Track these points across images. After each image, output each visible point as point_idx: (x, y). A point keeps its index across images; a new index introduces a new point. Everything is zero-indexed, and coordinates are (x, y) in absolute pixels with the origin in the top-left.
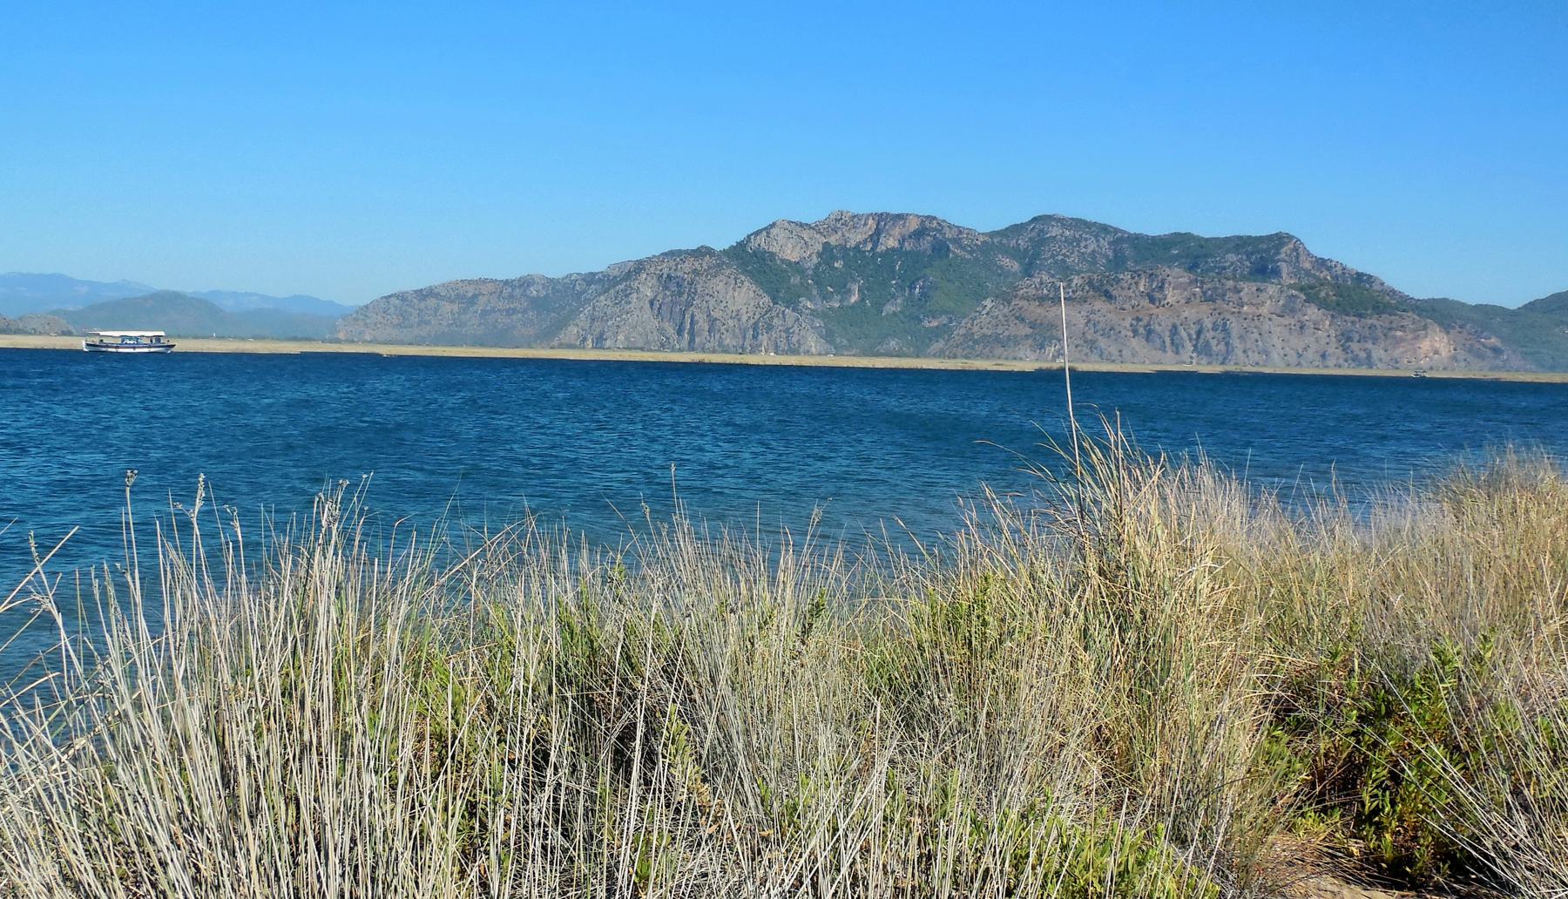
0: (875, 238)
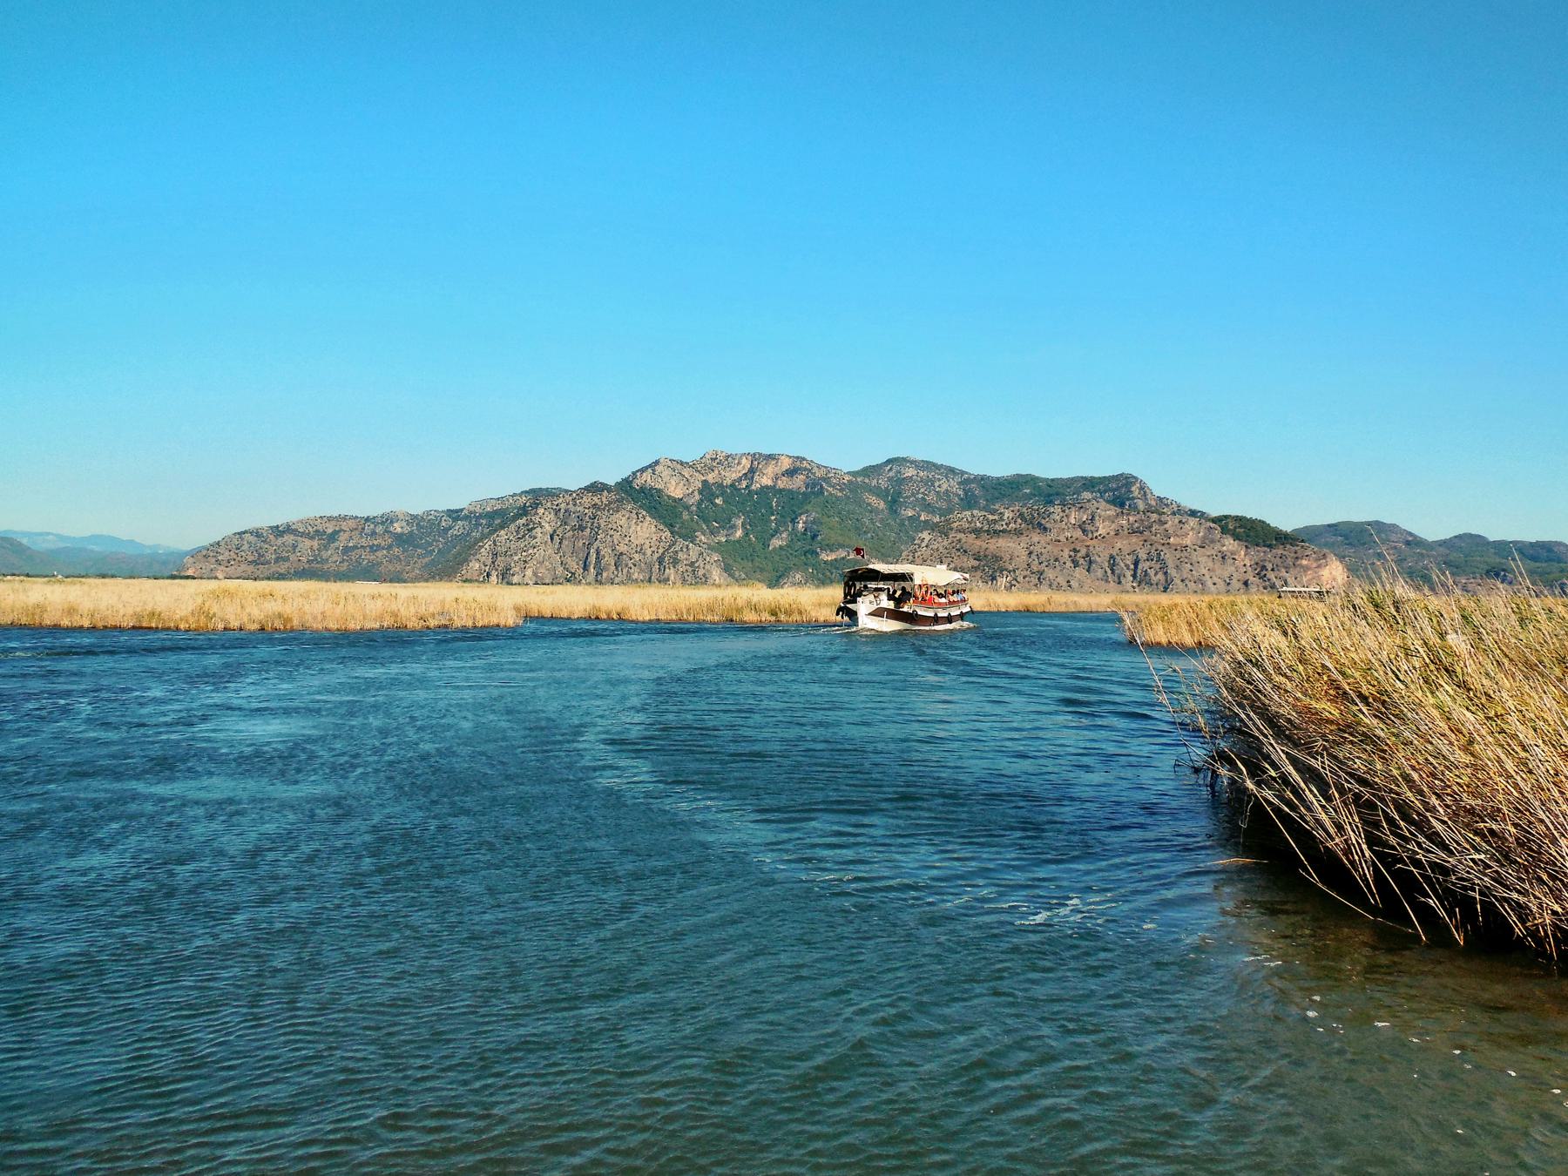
0: (749, 476)
